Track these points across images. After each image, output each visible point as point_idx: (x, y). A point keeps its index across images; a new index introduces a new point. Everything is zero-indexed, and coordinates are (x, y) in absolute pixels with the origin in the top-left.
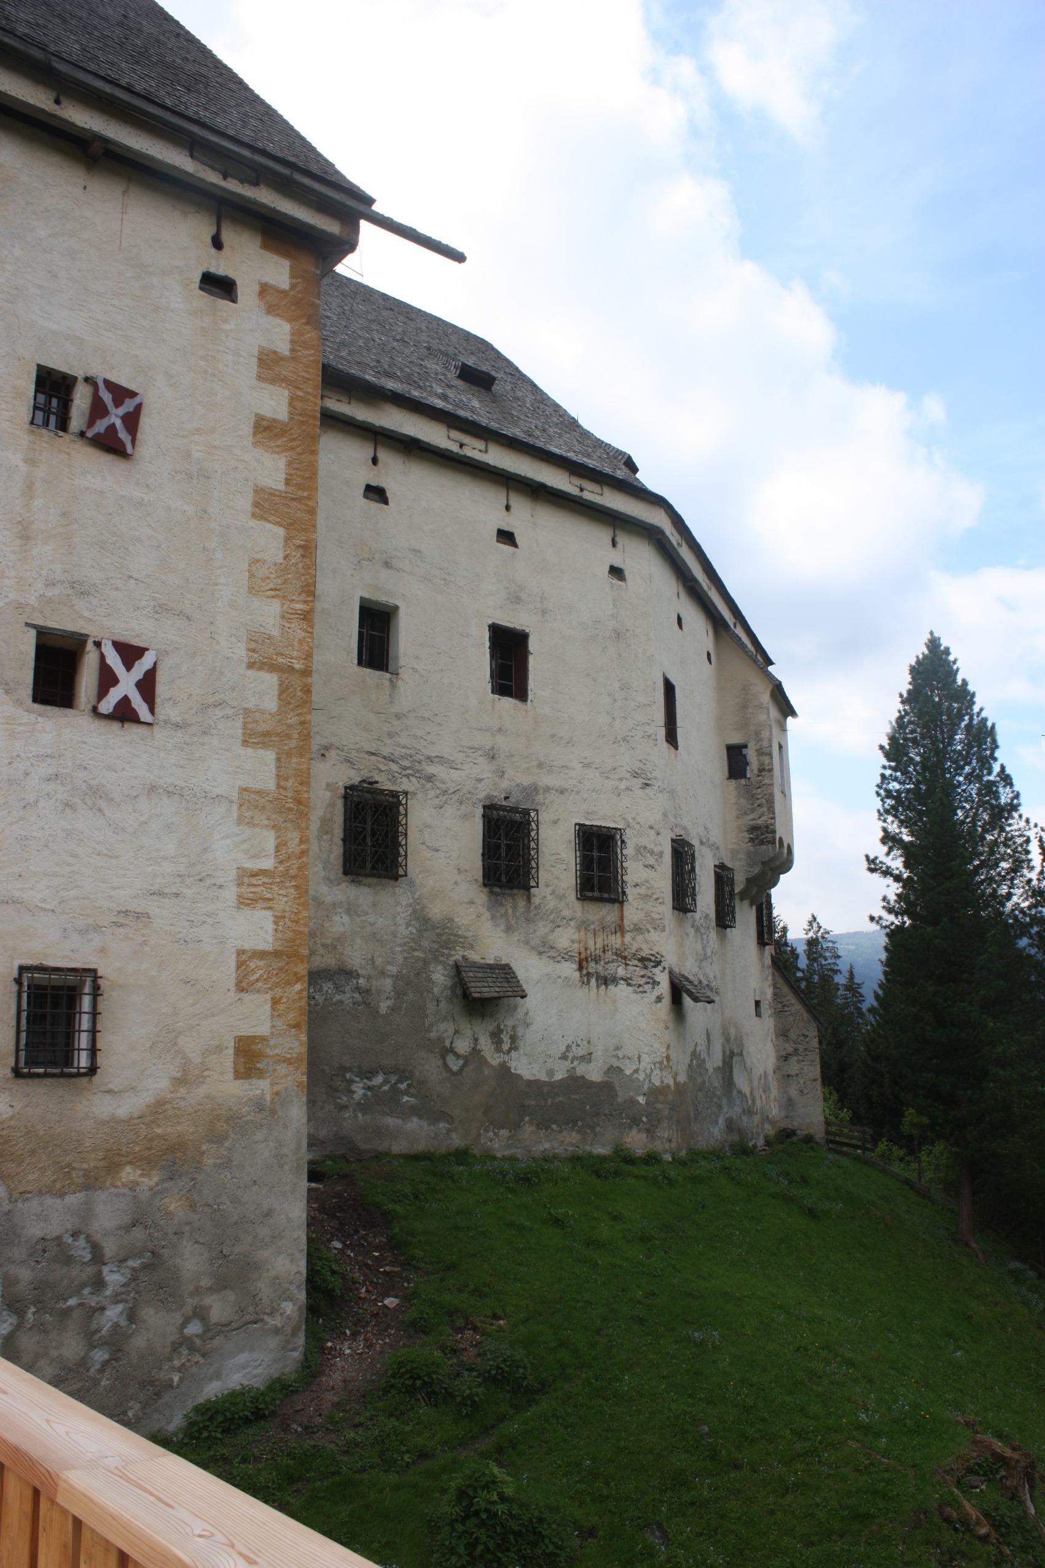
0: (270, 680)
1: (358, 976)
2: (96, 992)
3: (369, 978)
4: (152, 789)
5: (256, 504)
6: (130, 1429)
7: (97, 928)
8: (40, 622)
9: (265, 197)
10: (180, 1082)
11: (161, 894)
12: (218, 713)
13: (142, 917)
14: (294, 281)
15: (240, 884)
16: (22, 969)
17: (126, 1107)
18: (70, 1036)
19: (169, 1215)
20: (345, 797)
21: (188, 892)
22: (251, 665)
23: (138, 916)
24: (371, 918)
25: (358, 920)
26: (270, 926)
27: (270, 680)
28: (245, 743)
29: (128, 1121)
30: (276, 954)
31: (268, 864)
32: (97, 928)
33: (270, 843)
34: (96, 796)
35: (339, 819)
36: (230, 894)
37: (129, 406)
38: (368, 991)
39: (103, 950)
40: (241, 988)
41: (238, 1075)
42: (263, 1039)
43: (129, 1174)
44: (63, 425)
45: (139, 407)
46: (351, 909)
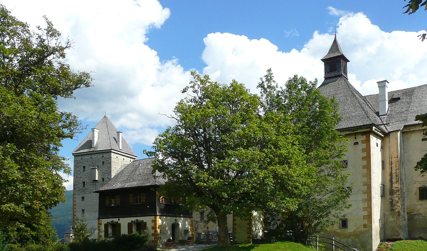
0: (366, 187)
1: (422, 214)
3: (424, 214)
5: (363, 167)
9: (359, 131)
10: (357, 228)
12: (359, 191)
15: (363, 208)
17: (351, 231)
19: (356, 241)
20: (419, 189)
22: (363, 186)
23: (351, 213)
24: (425, 206)
25: (422, 206)
26: (367, 212)
27: (366, 187)
28: (363, 194)
29: (352, 232)
30: (368, 215)
31: (367, 206)
33: (367, 204)
35: (418, 192)
36: (362, 210)
37: (346, 162)
38: (425, 216)
40: (363, 219)
41: (152, 220)
42: (367, 224)
43: (352, 237)
45: (347, 162)
46: (421, 205)
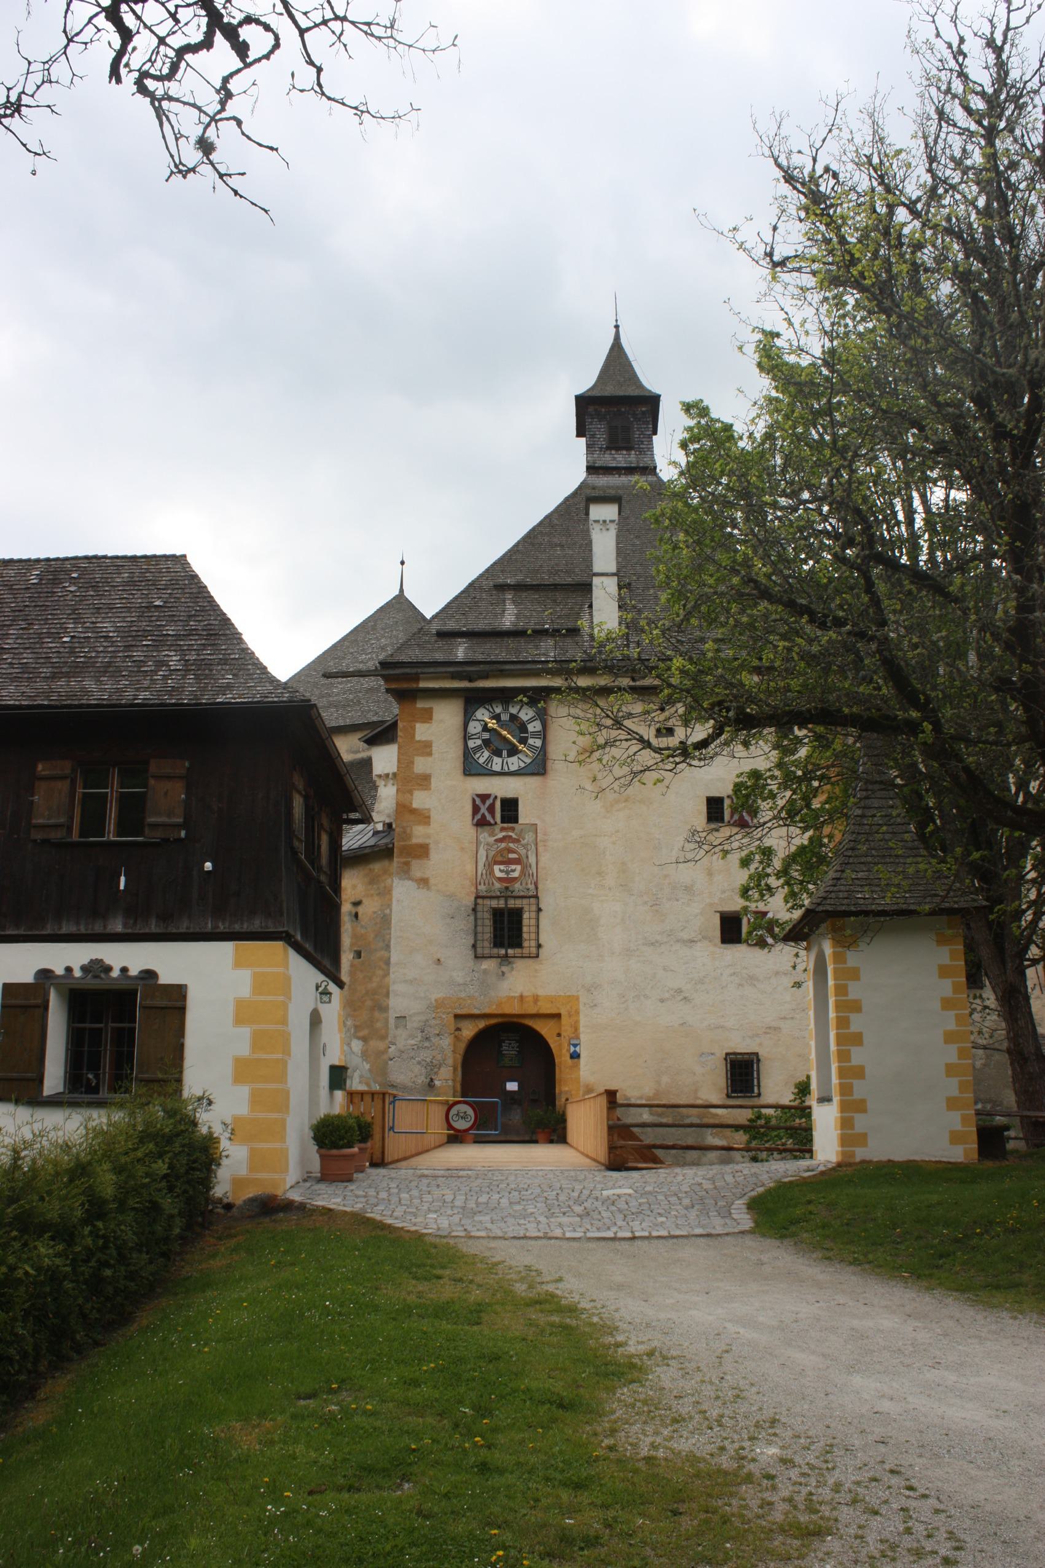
2: (759, 1060)
4: (777, 973)
6: (225, 614)
7: (757, 1035)
8: (720, 909)
11: (785, 1018)
13: (777, 1029)
14: (845, 1115)
16: (727, 1054)
18: (753, 1087)
21: (798, 1016)
23: (775, 1029)
32: (757, 1035)
34: (752, 979)
39: (760, 1044)
44: (722, 820)
